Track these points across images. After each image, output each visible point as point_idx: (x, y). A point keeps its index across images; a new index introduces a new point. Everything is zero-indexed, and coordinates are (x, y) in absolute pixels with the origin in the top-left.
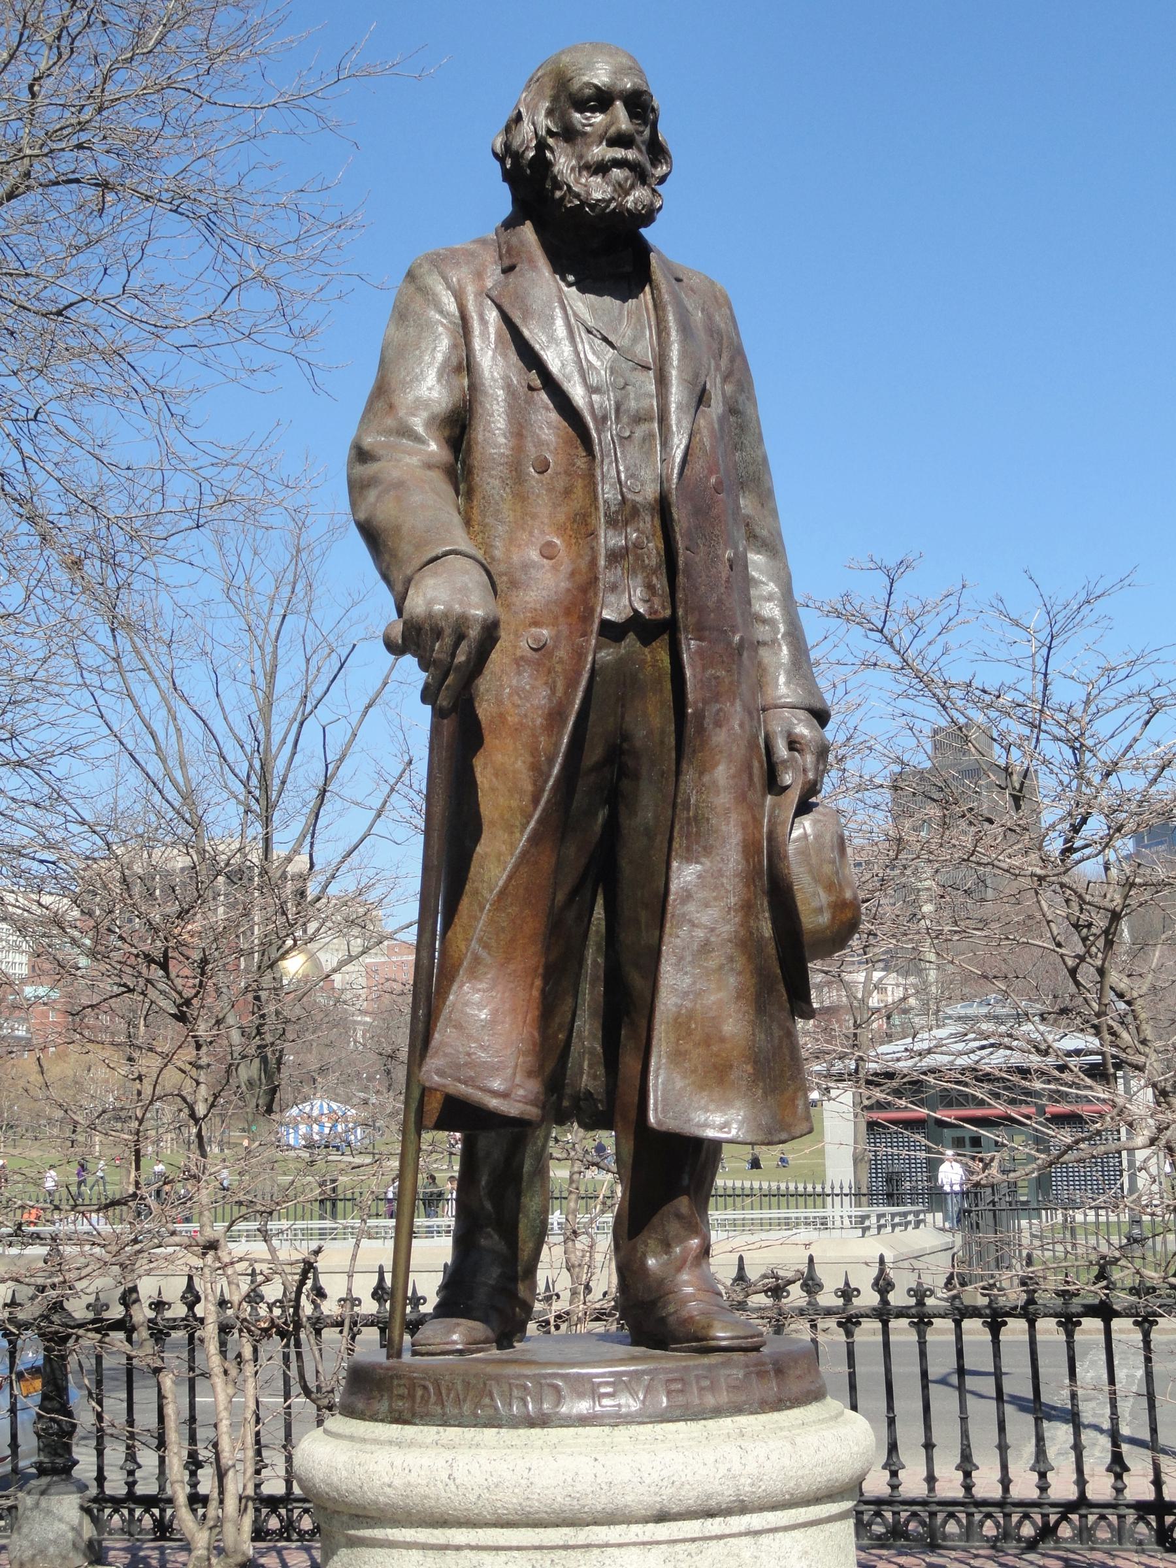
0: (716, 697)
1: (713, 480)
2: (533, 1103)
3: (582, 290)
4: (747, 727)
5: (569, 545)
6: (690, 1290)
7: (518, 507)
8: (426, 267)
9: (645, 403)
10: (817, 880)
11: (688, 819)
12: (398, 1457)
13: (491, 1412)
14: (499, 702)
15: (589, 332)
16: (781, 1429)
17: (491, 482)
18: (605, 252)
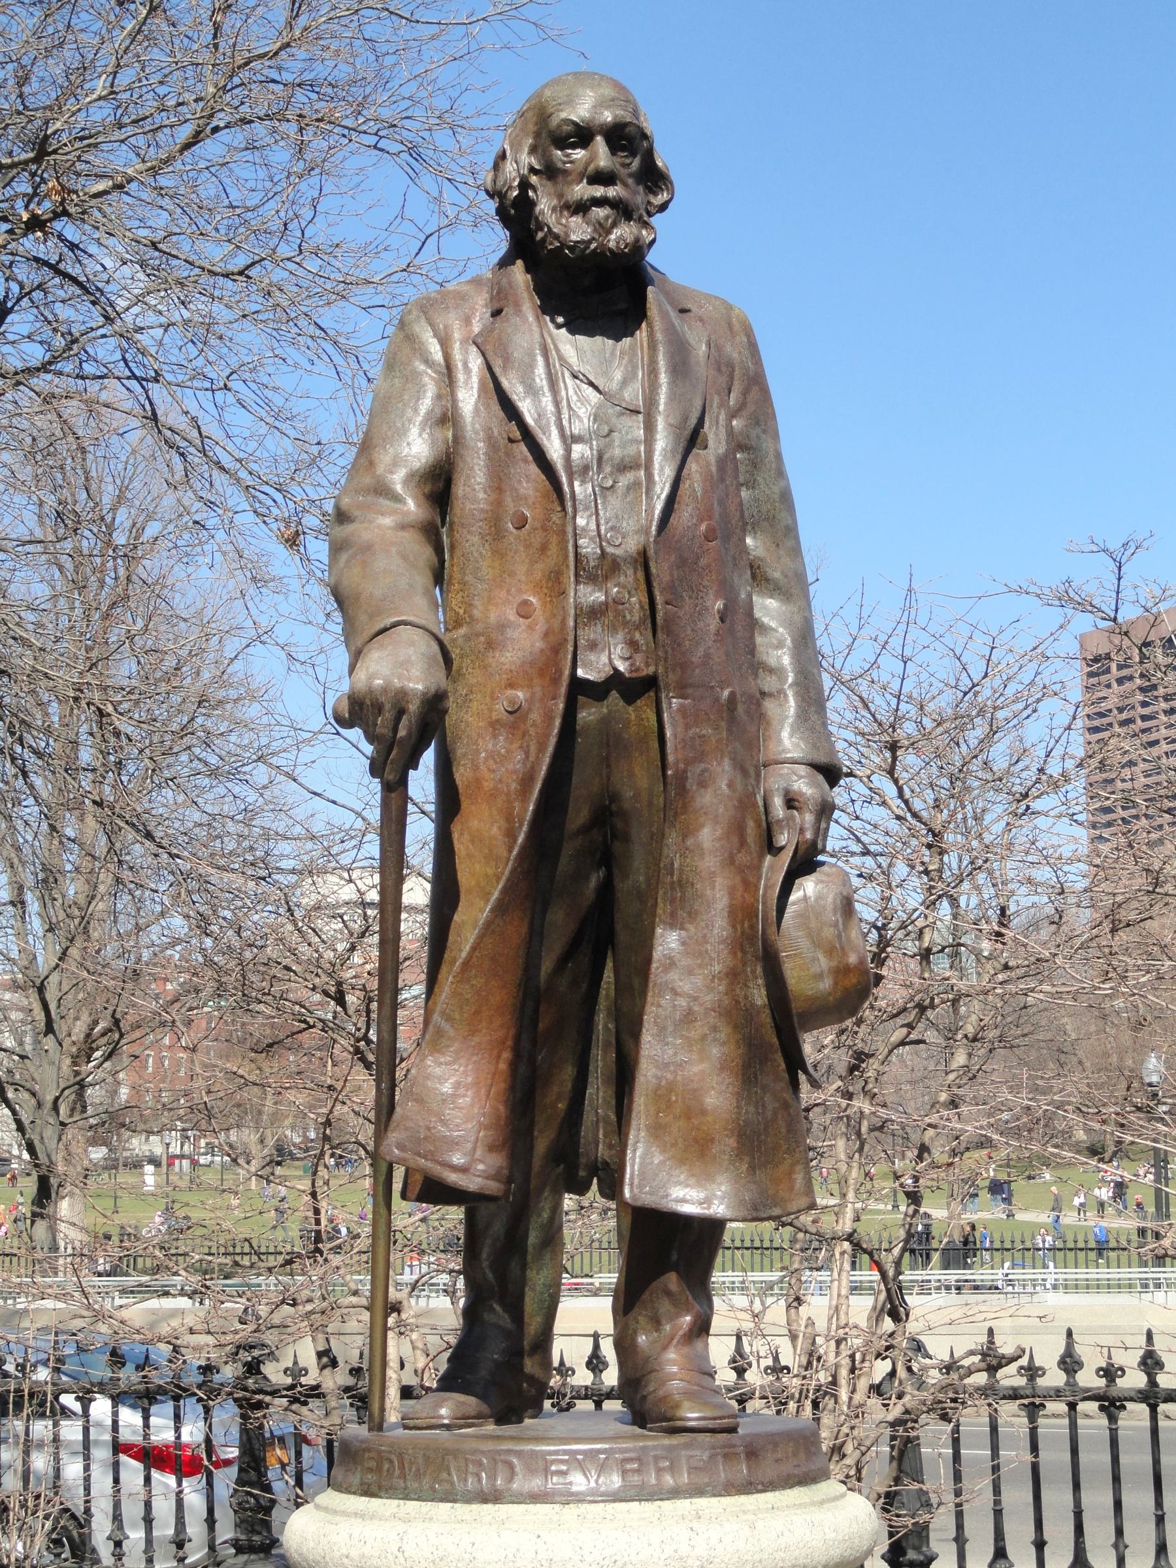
0: (701, 757)
1: (703, 527)
2: (495, 1177)
3: (573, 332)
4: (739, 786)
5: (544, 604)
6: (675, 1369)
7: (497, 564)
8: (415, 313)
9: (631, 450)
10: (817, 943)
11: (673, 883)
12: (357, 1527)
13: (447, 1486)
14: (476, 768)
15: (575, 377)
16: (745, 1512)
17: (470, 539)
18: (600, 291)
